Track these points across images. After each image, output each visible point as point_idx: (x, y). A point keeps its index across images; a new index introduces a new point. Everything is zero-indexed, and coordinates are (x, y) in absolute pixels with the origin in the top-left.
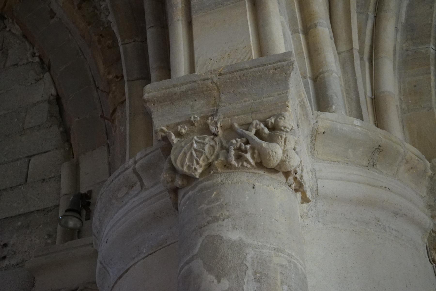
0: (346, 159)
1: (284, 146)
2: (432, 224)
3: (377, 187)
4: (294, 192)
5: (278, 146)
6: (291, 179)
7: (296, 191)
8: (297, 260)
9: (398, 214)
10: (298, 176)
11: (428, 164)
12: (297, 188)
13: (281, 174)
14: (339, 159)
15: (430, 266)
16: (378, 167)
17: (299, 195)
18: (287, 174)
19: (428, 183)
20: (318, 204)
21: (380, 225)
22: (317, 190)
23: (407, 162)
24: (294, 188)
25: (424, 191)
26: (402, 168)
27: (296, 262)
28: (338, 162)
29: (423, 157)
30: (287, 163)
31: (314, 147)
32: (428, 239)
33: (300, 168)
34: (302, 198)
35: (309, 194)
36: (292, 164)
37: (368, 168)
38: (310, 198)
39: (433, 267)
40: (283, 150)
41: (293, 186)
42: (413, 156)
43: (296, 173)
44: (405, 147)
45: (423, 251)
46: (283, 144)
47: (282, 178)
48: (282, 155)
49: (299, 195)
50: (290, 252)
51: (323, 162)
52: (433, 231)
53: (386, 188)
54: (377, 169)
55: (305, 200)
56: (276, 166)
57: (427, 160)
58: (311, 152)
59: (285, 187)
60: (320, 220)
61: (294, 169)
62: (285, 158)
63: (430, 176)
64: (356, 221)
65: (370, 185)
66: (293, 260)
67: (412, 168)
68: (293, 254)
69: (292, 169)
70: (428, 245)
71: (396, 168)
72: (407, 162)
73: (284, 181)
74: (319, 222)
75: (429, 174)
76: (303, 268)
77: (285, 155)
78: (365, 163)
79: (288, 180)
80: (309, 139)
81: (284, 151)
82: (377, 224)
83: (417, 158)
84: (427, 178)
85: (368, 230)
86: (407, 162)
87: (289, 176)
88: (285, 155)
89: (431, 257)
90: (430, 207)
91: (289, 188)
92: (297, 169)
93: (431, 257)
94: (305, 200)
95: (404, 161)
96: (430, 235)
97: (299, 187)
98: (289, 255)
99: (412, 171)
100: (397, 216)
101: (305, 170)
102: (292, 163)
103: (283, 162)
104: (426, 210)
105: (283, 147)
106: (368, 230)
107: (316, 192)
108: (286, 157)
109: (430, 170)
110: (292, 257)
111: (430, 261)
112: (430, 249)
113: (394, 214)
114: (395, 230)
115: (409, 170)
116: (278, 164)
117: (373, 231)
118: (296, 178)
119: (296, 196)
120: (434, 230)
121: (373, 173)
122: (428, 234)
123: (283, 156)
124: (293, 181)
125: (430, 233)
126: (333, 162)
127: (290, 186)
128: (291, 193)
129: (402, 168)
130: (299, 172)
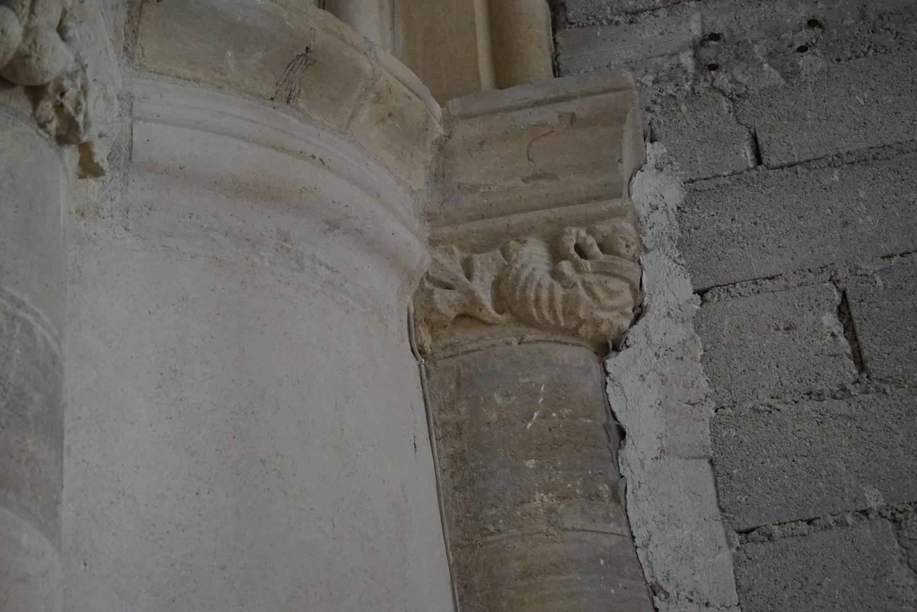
0: (217, 76)
1: (29, 18)
2: (428, 260)
3: (290, 152)
4: (54, 143)
5: (11, 15)
6: (47, 108)
7: (61, 140)
8: (37, 315)
9: (338, 228)
10: (69, 107)
11: (437, 109)
12: (64, 133)
13: (20, 90)
14: (199, 75)
15: (412, 363)
16: (302, 103)
17: (71, 155)
18: (36, 93)
19: (430, 158)
20: (131, 183)
21: (288, 250)
22: (131, 148)
23: (379, 98)
24: (54, 133)
25: (420, 179)
26: (365, 113)
27: (30, 318)
28: (197, 81)
29: (425, 91)
30: (33, 61)
31: (136, 37)
32: (415, 297)
33: (79, 82)
34: (81, 163)
35: (100, 154)
36: (46, 66)
37: (276, 103)
38: (105, 165)
39: (419, 366)
40: (26, 27)
41: (53, 126)
42: (397, 86)
43: (63, 94)
44: (377, 60)
45: (398, 325)
46: (26, 10)
47: (22, 104)
48: (20, 39)
49: (71, 155)
50: (16, 293)
51: (156, 77)
52: (428, 278)
53: (314, 157)
54: (298, 109)
55: (89, 168)
56: (5, 69)
57: (436, 98)
58: (126, 49)
59: (30, 128)
60: (131, 226)
61: (55, 81)
62: (27, 49)
63: (436, 140)
64: (227, 234)
65: (273, 147)
66: (21, 313)
67: (390, 115)
68: (26, 299)
69: (49, 78)
70: (412, 310)
71: (349, 111)
72: (379, 98)
73: (28, 111)
74: (126, 229)
75: (436, 136)
76: (49, 338)
77: (30, 41)
78: (267, 89)
79: (39, 109)
80: (123, 16)
81: (29, 31)
82: (282, 247)
83: (406, 91)
84: (429, 145)
85: (257, 260)
86: (378, 99)
87: (42, 98)
88: (30, 41)
89: (417, 339)
90: (429, 216)
91: (41, 131)
92: (66, 83)
93: (417, 339)
94: (89, 168)
95: (371, 95)
96: (422, 288)
97: (68, 133)
98: (12, 299)
99: (389, 122)
100: (336, 231)
101: (94, 91)
102: (46, 64)
103: (22, 57)
104: (418, 225)
105: (26, 18)
106: (257, 260)
107: (125, 153)
108: (30, 47)
109: (438, 126)
110: (20, 305)
111: (413, 351)
112: (415, 320)
113: (327, 227)
114: (328, 267)
115: (383, 120)
116: (11, 64)
117: (267, 264)
118: (62, 106)
119: (61, 157)
120: (431, 274)
121: (286, 116)
122: (415, 285)
123: (24, 41)
124: (53, 113)
125: (422, 281)
126: (182, 81)
127: (42, 126)
128: (44, 145)
129: (365, 113)
130: (71, 93)
